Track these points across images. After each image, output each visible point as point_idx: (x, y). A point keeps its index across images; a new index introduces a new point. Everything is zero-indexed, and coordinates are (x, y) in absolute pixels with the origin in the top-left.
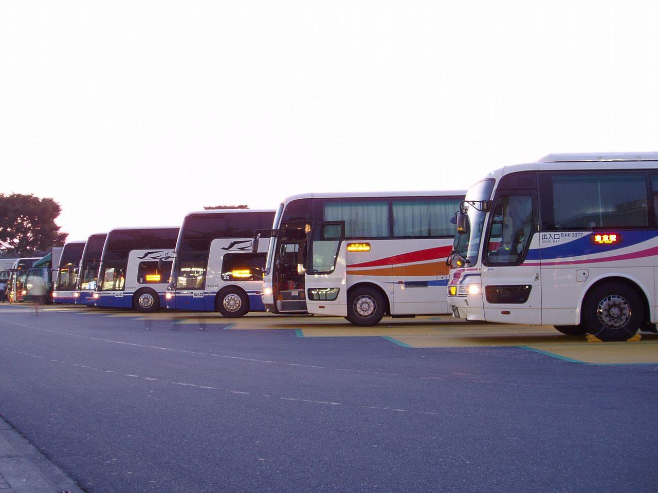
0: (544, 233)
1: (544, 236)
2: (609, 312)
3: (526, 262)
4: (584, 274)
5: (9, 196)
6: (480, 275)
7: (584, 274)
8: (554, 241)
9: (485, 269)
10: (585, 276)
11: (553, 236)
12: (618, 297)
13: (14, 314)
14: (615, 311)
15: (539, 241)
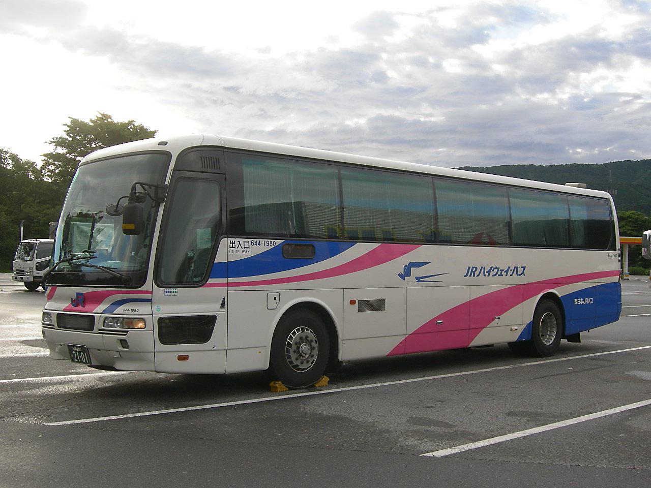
0: (233, 240)
1: (232, 243)
2: (298, 348)
3: (211, 281)
4: (275, 298)
5: (116, 122)
6: (150, 301)
7: (275, 298)
8: (243, 252)
9: (159, 292)
10: (276, 301)
11: (242, 243)
12: (311, 332)
13: (560, 419)
14: (304, 347)
15: (233, 250)
